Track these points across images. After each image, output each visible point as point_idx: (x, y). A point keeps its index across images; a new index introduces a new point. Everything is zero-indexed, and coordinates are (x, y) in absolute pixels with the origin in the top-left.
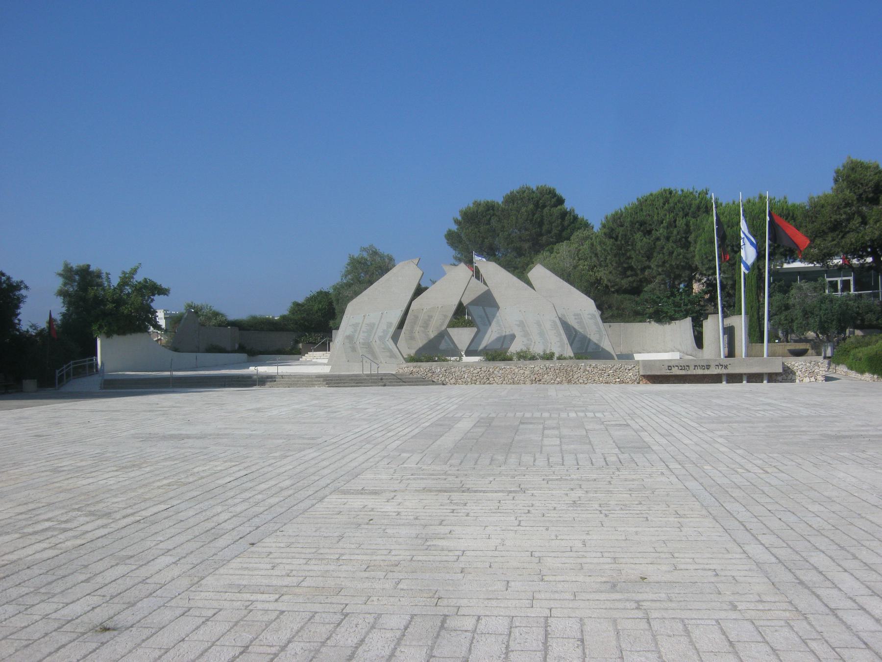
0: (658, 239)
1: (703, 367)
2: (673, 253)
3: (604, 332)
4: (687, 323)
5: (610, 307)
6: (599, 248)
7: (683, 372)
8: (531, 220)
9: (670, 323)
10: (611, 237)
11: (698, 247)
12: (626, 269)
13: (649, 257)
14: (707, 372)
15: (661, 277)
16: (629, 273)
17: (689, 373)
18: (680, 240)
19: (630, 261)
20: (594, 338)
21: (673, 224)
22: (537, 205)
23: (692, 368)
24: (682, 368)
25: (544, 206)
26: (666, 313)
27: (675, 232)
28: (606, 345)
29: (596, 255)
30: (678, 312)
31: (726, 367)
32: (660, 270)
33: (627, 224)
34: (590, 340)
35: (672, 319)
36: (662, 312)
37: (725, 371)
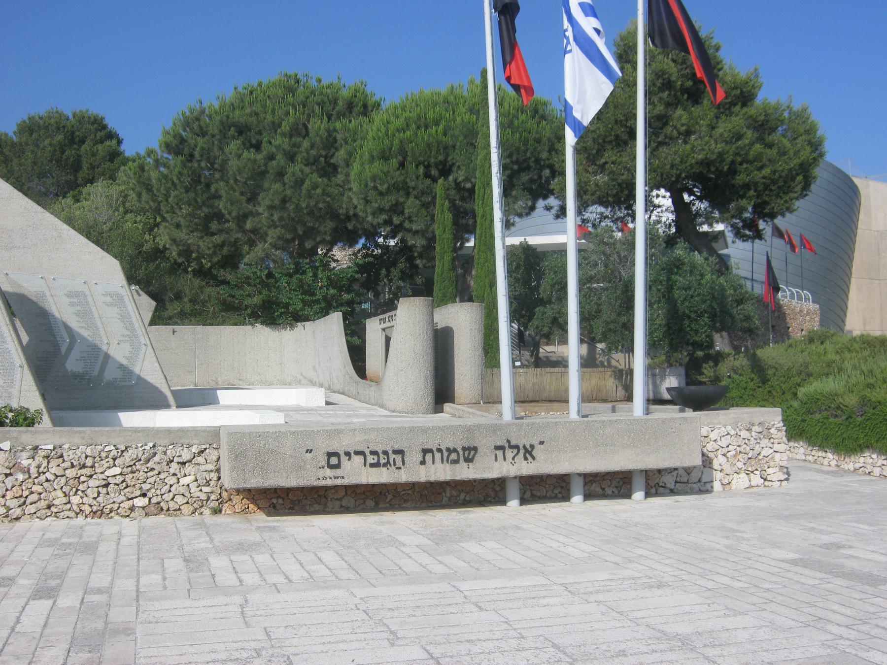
0: (272, 157)
1: (451, 455)
2: (302, 181)
3: (143, 340)
4: (335, 321)
5: (178, 297)
6: (154, 175)
7: (381, 476)
8: (59, 161)
9: (292, 327)
10: (177, 152)
11: (356, 168)
12: (208, 219)
13: (253, 199)
14: (465, 472)
15: (278, 230)
16: (214, 226)
17: (404, 476)
18: (316, 160)
19: (216, 202)
20: (119, 353)
21: (300, 130)
22: (72, 141)
23: (413, 457)
24: (380, 459)
25: (82, 142)
26: (287, 306)
27: (306, 144)
28: (148, 370)
29: (149, 188)
30: (309, 304)
31: (529, 453)
32: (276, 217)
33: (214, 129)
34: (107, 356)
35: (298, 318)
36: (278, 304)
37: (527, 468)
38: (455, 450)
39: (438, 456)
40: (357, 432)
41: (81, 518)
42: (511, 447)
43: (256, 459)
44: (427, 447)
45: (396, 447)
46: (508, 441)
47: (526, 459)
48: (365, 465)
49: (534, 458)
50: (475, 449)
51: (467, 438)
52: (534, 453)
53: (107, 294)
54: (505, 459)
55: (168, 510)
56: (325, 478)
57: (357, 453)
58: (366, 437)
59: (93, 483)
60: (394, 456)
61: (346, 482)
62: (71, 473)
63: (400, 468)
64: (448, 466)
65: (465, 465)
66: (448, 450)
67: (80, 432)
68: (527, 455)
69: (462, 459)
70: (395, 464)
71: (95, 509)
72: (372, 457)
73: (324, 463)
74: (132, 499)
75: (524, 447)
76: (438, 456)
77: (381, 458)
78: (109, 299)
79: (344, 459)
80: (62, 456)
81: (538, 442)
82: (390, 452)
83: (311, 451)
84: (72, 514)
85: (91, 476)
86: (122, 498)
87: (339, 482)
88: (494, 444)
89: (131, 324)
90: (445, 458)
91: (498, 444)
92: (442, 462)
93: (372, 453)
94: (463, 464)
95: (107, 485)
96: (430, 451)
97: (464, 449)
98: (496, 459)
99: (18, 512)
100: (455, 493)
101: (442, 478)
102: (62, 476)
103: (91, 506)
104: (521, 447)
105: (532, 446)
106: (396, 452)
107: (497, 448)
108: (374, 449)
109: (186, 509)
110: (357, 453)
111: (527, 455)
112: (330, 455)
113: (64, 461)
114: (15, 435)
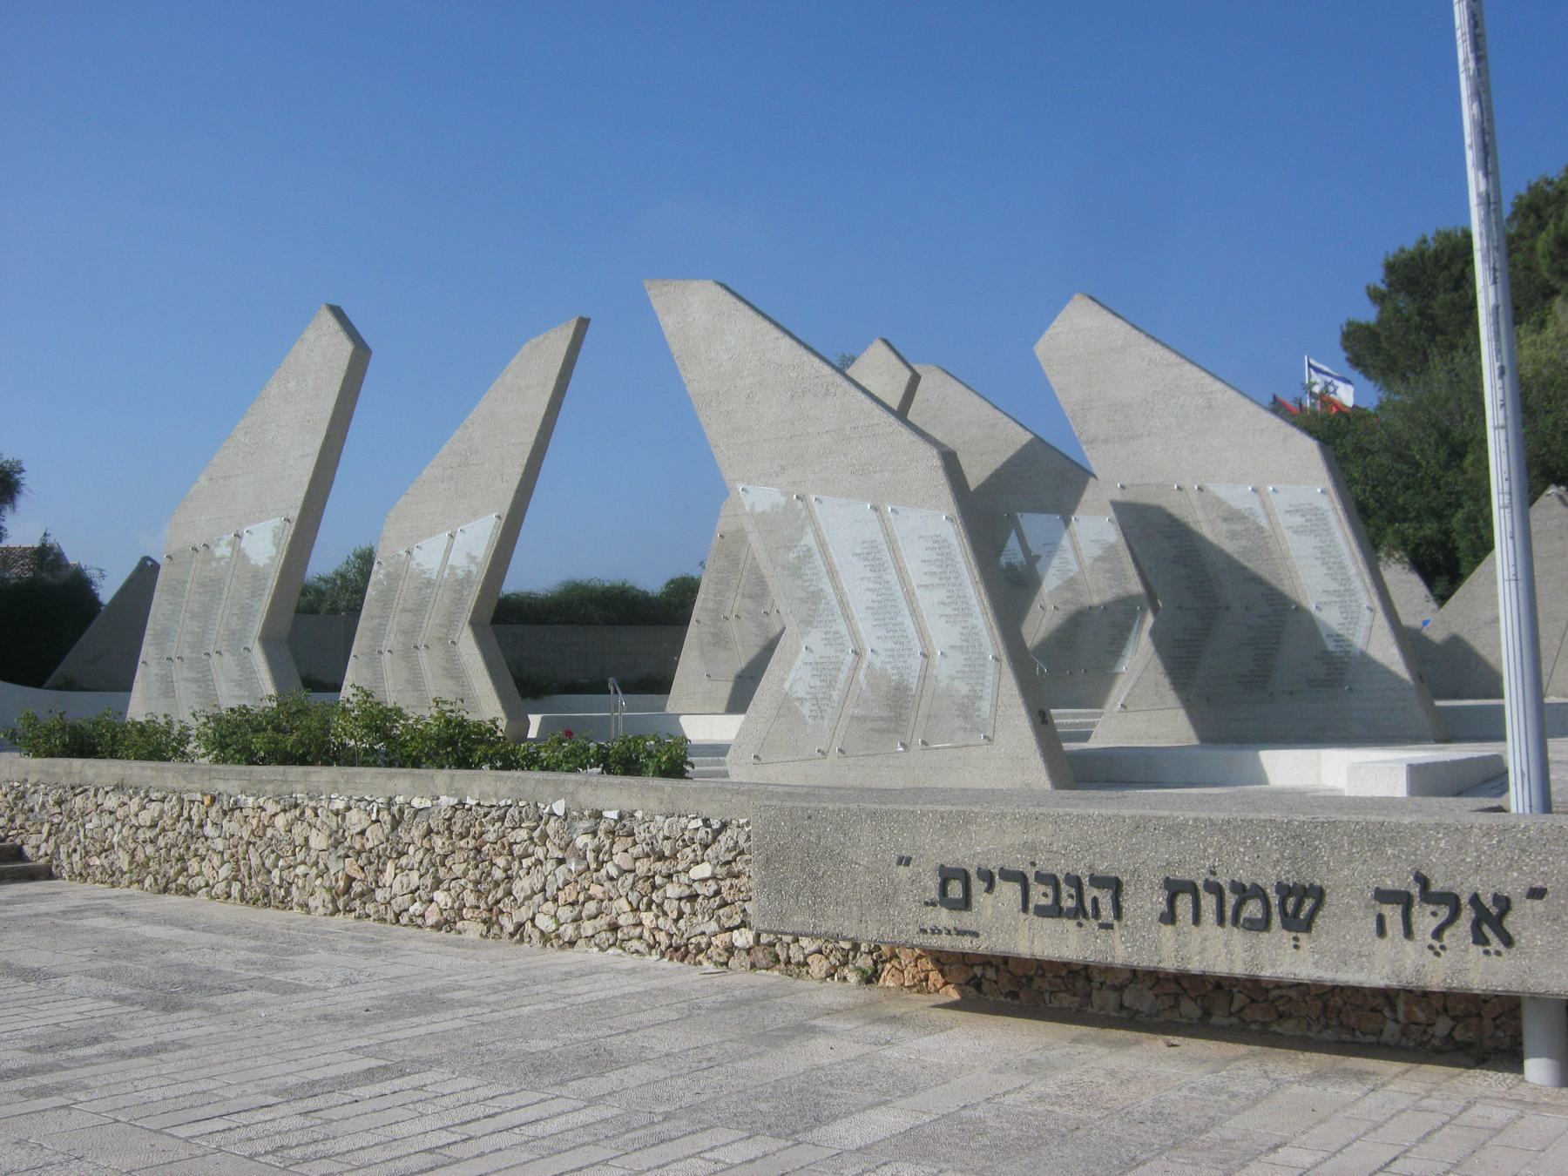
1: (1240, 904)
14: (1286, 959)
23: (1145, 901)
31: (1491, 921)
38: (1258, 892)
39: (1208, 902)
40: (1007, 822)
41: (655, 956)
42: (1428, 896)
43: (803, 870)
44: (1180, 874)
45: (1102, 868)
46: (1423, 881)
47: (1480, 939)
48: (1025, 909)
49: (1508, 941)
50: (1319, 894)
51: (1294, 859)
52: (1510, 923)
53: (1296, 510)
54: (1408, 933)
55: (788, 962)
56: (936, 931)
57: (1008, 875)
58: (1028, 837)
59: (673, 890)
60: (1095, 892)
61: (982, 945)
62: (642, 867)
63: (1110, 927)
64: (1238, 937)
65: (1287, 937)
66: (1238, 888)
67: (657, 789)
68: (1486, 929)
69: (1276, 919)
70: (1097, 915)
71: (676, 941)
72: (1042, 888)
73: (934, 894)
74: (731, 929)
75: (1475, 900)
76: (1208, 902)
77: (1064, 895)
78: (1298, 520)
79: (978, 886)
80: (631, 834)
81: (1522, 889)
82: (1085, 881)
83: (908, 863)
84: (642, 947)
85: (669, 876)
86: (713, 926)
87: (966, 944)
88: (1374, 883)
89: (1342, 567)
90: (1229, 913)
91: (1389, 884)
92: (1221, 921)
93: (1041, 878)
94: (1279, 936)
95: (693, 898)
96: (1191, 888)
97: (1284, 890)
98: (1381, 931)
99: (568, 931)
100: (1421, 1016)
101: (1221, 968)
102: (631, 871)
103: (671, 936)
104: (1464, 900)
105: (1504, 904)
106: (1097, 881)
107: (1383, 896)
108: (1048, 868)
109: (818, 966)
110: (1008, 875)
111: (1486, 929)
112: (945, 875)
113: (635, 843)
114: (570, 788)
